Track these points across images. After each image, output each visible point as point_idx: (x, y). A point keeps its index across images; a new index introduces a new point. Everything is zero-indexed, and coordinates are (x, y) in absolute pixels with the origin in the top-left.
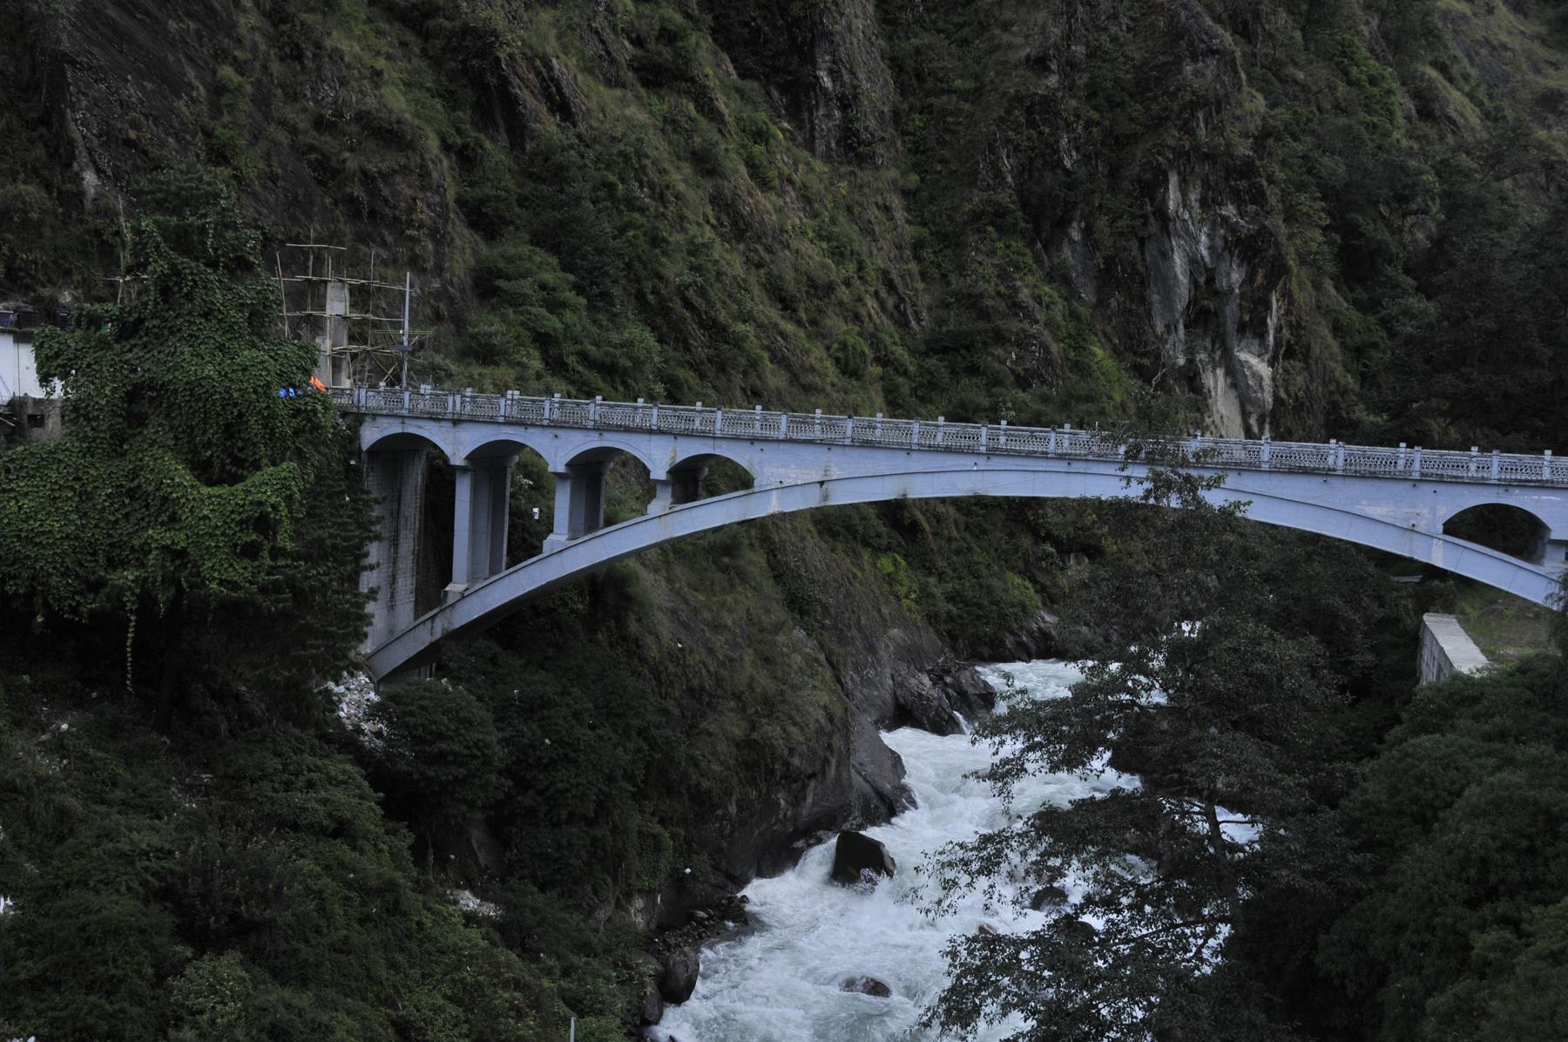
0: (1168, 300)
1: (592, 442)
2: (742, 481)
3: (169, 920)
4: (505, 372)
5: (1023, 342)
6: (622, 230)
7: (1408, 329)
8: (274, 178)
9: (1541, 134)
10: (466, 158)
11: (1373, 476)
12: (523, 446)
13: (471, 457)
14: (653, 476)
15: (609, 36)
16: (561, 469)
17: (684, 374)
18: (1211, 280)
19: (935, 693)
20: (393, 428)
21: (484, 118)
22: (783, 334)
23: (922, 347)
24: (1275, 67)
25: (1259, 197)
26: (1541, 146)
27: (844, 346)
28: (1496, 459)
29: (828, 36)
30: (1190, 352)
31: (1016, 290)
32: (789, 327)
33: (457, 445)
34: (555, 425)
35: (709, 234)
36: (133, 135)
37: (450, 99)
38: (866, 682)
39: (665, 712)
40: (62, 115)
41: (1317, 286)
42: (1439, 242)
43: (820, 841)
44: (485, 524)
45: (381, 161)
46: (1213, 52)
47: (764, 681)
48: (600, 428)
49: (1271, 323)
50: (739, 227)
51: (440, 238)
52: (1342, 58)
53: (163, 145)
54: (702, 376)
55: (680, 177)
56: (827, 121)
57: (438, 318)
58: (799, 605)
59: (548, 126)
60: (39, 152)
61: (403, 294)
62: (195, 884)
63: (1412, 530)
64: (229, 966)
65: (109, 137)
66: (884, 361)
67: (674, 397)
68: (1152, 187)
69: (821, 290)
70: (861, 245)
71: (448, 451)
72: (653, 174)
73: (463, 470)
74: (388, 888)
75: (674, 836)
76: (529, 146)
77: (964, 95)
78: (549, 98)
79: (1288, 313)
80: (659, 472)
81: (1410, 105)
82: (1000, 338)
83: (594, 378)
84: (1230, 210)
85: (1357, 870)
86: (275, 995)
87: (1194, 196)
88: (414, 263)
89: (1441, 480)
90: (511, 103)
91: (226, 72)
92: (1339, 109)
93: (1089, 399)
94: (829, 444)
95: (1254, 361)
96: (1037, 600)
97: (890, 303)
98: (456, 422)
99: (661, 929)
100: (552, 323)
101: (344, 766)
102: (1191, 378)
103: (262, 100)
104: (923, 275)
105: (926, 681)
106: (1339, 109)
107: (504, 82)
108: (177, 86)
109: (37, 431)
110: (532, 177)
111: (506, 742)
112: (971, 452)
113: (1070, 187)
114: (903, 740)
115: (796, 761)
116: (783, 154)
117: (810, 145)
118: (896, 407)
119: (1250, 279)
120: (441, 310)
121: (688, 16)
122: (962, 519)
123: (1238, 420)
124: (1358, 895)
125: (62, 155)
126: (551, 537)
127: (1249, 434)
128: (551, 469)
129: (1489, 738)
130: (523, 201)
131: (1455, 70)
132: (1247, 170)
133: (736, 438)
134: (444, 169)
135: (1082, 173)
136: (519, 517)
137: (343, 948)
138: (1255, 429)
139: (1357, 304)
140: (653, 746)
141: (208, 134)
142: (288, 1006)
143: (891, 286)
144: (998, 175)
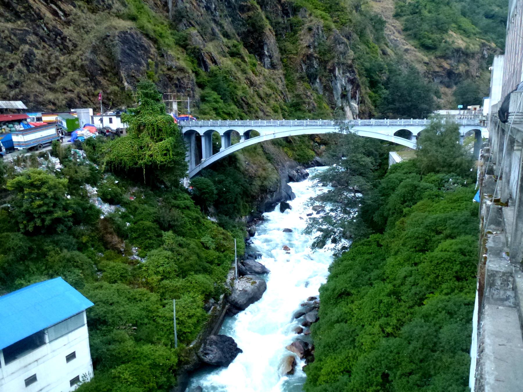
0: (337, 93)
1: (228, 129)
2: (256, 134)
3: (158, 226)
4: (208, 116)
5: (309, 104)
6: (229, 86)
7: (383, 96)
8: (160, 81)
9: (405, 57)
10: (197, 74)
11: (380, 125)
15: (223, 47)
16: (222, 135)
17: (243, 114)
18: (345, 89)
19: (296, 174)
20: (188, 129)
21: (199, 65)
22: (262, 105)
23: (289, 106)
24: (354, 45)
25: (353, 72)
26: (405, 59)
27: (274, 106)
28: (403, 120)
29: (266, 44)
30: (342, 103)
31: (307, 93)
32: (263, 104)
33: (201, 131)
34: (220, 126)
35: (246, 86)
36: (133, 75)
37: (193, 62)
38: (283, 173)
39: (245, 181)
41: (366, 89)
42: (388, 79)
43: (277, 204)
44: (208, 146)
45: (180, 75)
46: (343, 43)
47: (264, 174)
48: (229, 126)
49: (357, 96)
50: (252, 84)
51: (193, 90)
52: (367, 43)
53: (139, 76)
54: (247, 114)
55: (239, 74)
56: (267, 61)
57: (194, 106)
58: (269, 159)
59: (212, 66)
60: (117, 80)
61: (187, 102)
62: (162, 219)
63: (388, 135)
64: (170, 233)
65: (128, 76)
66: (282, 109)
67: (242, 119)
68: (332, 71)
69: (268, 95)
70: (276, 86)
71: (199, 132)
72: (234, 74)
74: (197, 219)
75: (249, 205)
76: (209, 70)
77: (294, 54)
78: (211, 60)
79: (360, 94)
80: (241, 134)
81: (381, 52)
82: (304, 103)
83: (226, 116)
84: (348, 74)
85: (382, 200)
86: (180, 238)
87: (341, 72)
88: (189, 95)
89: (393, 125)
91: (150, 60)
92: (367, 53)
93: (322, 114)
94: (275, 126)
96: (315, 154)
97: (283, 97)
98: (201, 127)
99: (248, 222)
100: (216, 105)
101: (186, 196)
102: (342, 109)
103: (157, 65)
104: (289, 91)
105: (295, 172)
106: (367, 53)
107: (203, 58)
108: (140, 64)
109: (122, 135)
110: (210, 76)
111: (216, 189)
112: (303, 126)
113: (316, 71)
114: (291, 184)
115: (271, 189)
116: (259, 68)
117: (264, 66)
118: (285, 118)
119: (353, 88)
120: (196, 105)
121: (238, 42)
122: (299, 139)
124: (382, 205)
125: (121, 80)
127: (354, 119)
129: (404, 174)
130: (208, 81)
131: (389, 45)
132: (351, 66)
133: (256, 126)
134: (193, 76)
135: (319, 68)
136: (214, 144)
137: (190, 229)
139: (373, 92)
140: (244, 187)
141: (147, 73)
142: (182, 240)
143: (282, 93)
144: (302, 69)
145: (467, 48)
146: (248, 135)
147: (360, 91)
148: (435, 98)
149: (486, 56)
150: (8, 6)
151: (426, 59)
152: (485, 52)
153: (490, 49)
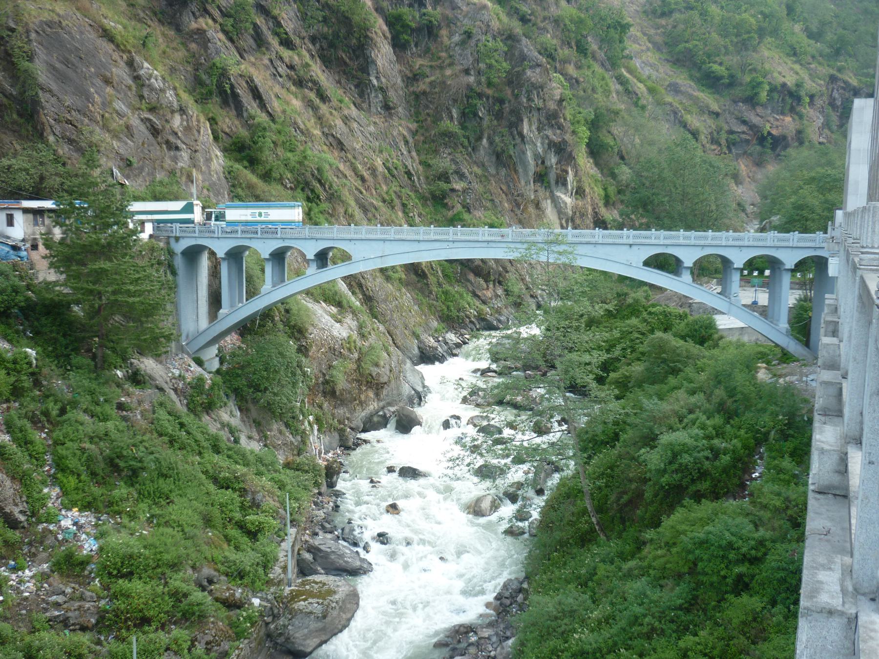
2: (346, 257)
12: (249, 247)
13: (226, 254)
14: (218, 256)
16: (267, 256)
40: (38, 112)
63: (630, 265)
73: (223, 259)
80: (310, 256)
87: (534, 128)
90: (235, 96)
95: (563, 196)
102: (537, 206)
123: (558, 221)
126: (221, 311)
128: (263, 257)
138: (565, 225)
145: (799, 85)
146: (322, 258)
147: (576, 168)
148: (733, 186)
149: (839, 103)
150: (854, 651)
151: (715, 107)
152: (836, 95)
153: (847, 86)
